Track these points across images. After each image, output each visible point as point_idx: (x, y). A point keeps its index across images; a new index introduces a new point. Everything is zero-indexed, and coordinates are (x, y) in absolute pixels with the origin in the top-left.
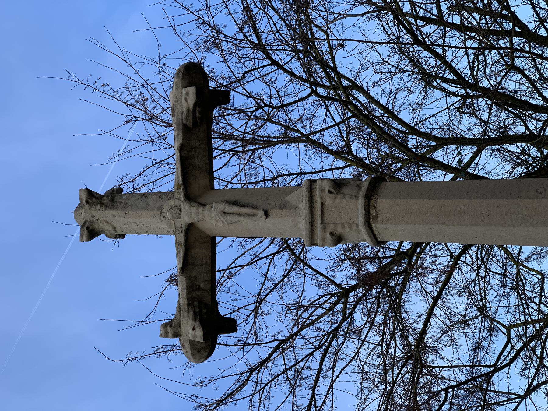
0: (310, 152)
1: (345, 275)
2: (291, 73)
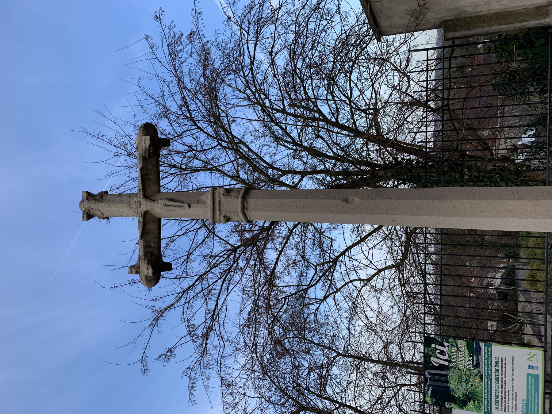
0: (218, 175)
1: (235, 240)
2: (208, 134)
